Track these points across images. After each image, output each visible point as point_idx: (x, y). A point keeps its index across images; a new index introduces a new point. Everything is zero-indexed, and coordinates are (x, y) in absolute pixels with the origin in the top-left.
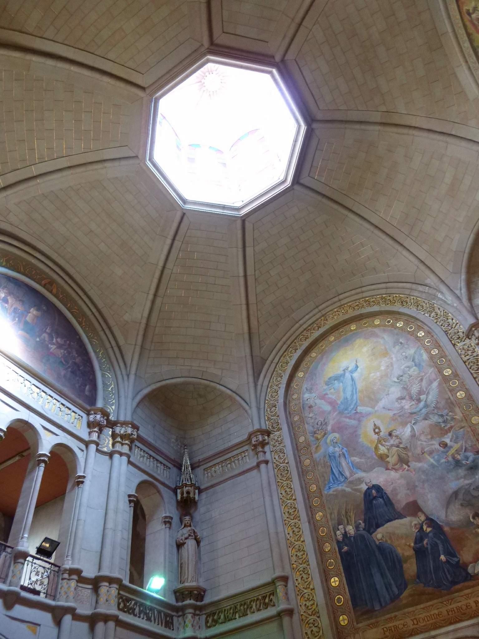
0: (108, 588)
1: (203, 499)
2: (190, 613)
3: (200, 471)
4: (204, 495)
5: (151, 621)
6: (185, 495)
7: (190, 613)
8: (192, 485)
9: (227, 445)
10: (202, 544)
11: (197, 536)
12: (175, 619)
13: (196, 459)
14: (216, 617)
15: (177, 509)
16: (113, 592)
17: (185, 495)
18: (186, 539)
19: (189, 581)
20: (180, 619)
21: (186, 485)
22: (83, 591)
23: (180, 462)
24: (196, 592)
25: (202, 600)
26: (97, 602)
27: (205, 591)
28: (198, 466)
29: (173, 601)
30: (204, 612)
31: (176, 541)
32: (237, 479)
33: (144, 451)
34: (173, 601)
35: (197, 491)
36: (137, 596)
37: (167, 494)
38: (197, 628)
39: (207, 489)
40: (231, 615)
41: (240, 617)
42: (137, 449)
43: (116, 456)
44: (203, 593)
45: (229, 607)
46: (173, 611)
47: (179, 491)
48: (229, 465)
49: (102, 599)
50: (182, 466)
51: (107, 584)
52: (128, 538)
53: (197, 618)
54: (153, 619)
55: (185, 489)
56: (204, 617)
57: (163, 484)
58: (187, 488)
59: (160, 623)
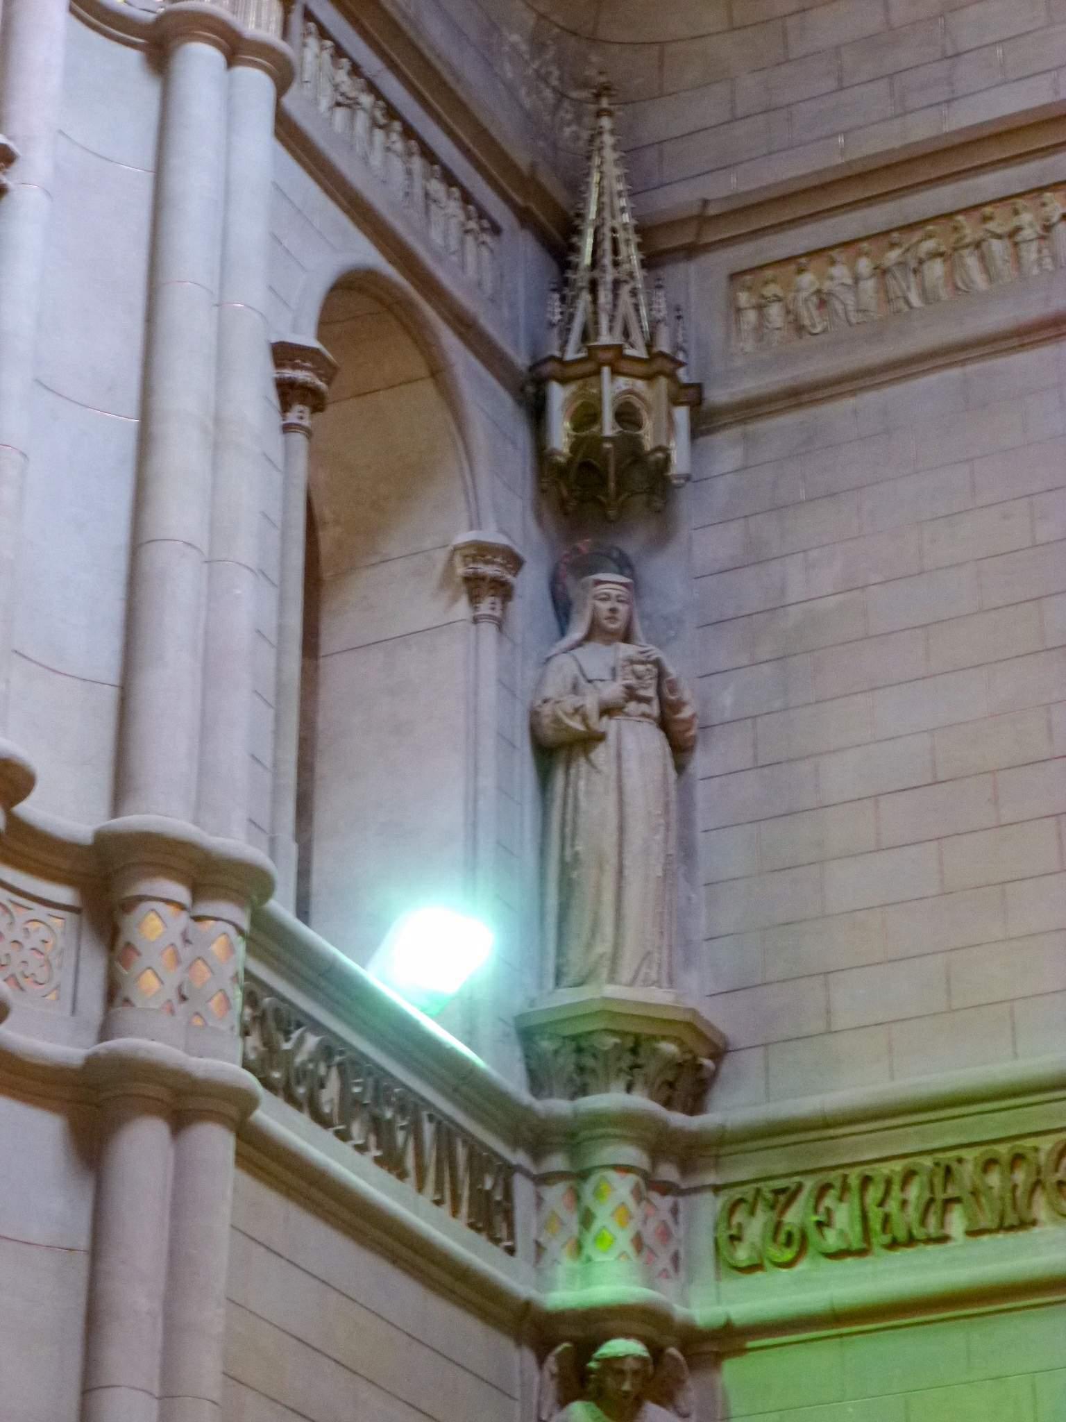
0: (183, 919)
1: (717, 477)
2: (625, 1169)
3: (699, 281)
4: (726, 450)
5: (402, 1175)
6: (609, 427)
7: (625, 1169)
8: (658, 365)
9: (922, 129)
10: (700, 763)
11: (678, 706)
12: (523, 1189)
13: (679, 198)
14: (793, 1217)
15: (539, 518)
16: (217, 948)
17: (609, 427)
18: (608, 710)
19: (626, 974)
20: (556, 1194)
21: (618, 361)
22: (21, 916)
23: (561, 196)
24: (669, 1048)
25: (695, 1105)
26: (113, 993)
27: (719, 1053)
28: (691, 251)
29: (510, 1078)
30: (711, 1178)
31: (534, 715)
32: (999, 363)
33: (355, 70)
34: (510, 1078)
35: (682, 414)
36: (333, 1006)
37: (486, 403)
38: (664, 1262)
39: (751, 409)
40: (913, 1214)
41: (973, 1233)
42: (313, 42)
43: (200, 60)
44: (707, 1063)
45: (898, 1166)
46: (515, 1142)
47: (558, 395)
48: (936, 269)
49: (150, 984)
50: (578, 232)
51: (180, 892)
52: (281, 629)
53: (664, 1203)
54: (410, 1162)
55: (611, 388)
56: (708, 1207)
57: (465, 326)
58: (623, 383)
59: (448, 1197)
